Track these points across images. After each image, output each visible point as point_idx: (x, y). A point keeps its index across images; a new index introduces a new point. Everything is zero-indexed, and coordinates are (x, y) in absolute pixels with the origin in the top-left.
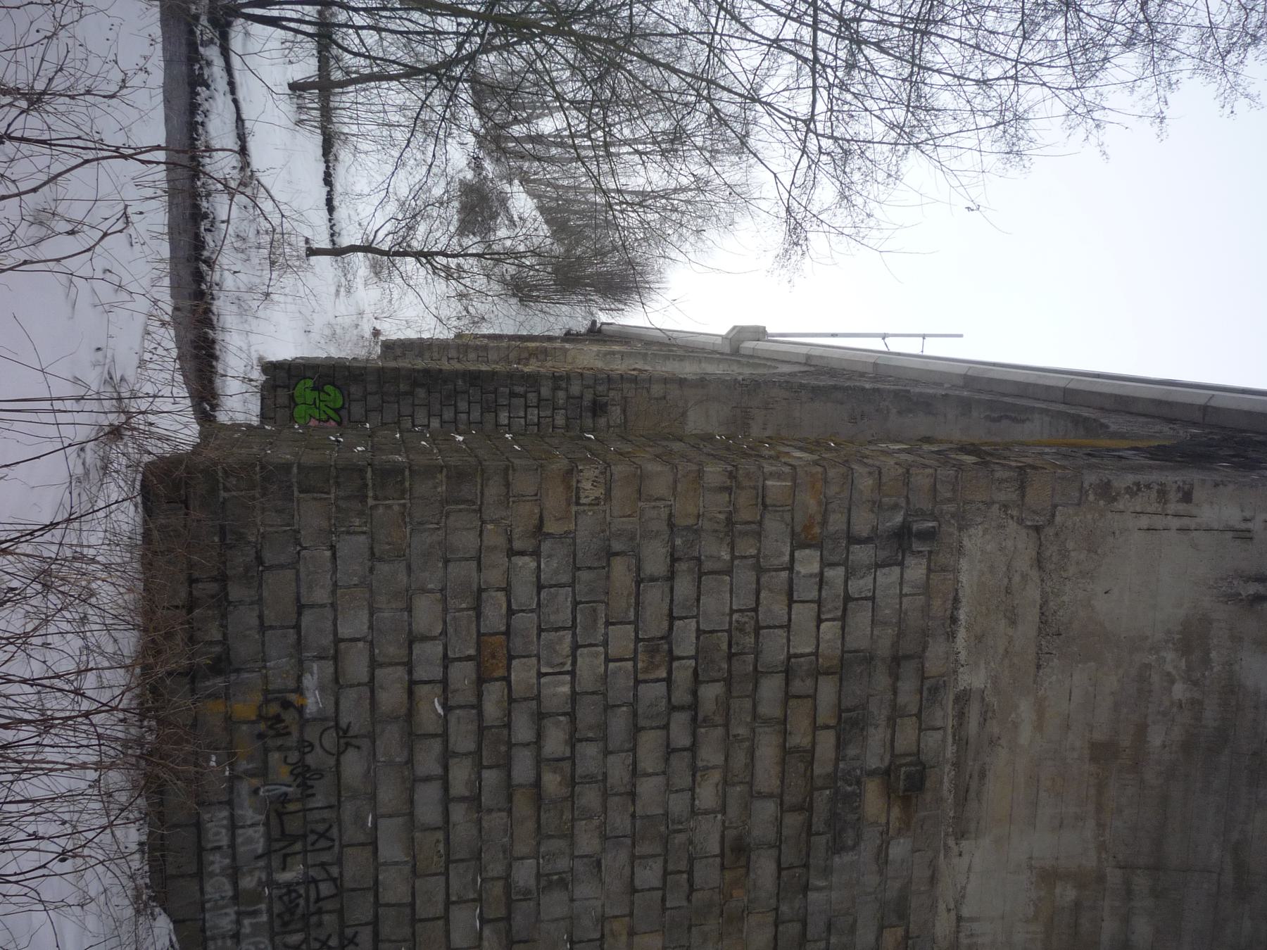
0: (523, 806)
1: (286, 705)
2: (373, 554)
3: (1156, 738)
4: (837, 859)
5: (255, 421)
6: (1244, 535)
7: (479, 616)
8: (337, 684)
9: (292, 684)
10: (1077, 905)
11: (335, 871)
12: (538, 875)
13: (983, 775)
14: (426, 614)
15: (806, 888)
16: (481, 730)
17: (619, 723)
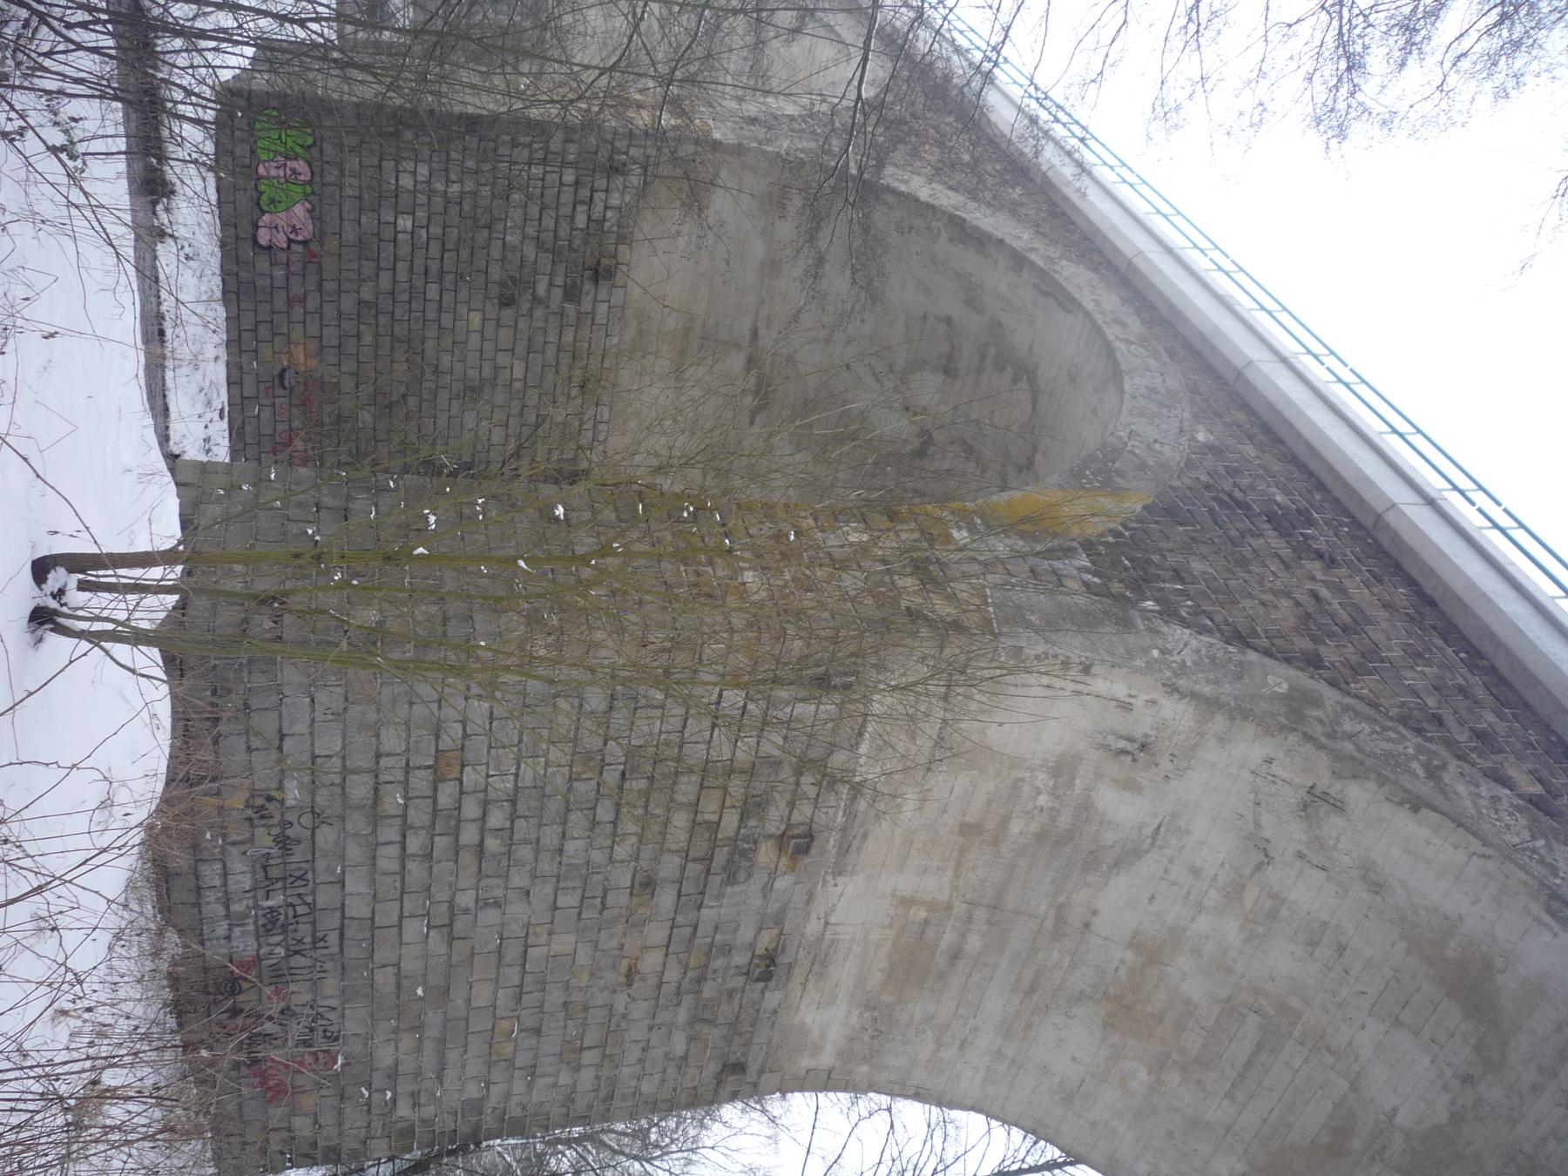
0: (467, 858)
1: (269, 799)
2: (347, 700)
3: (1016, 827)
4: (729, 889)
6: (1126, 707)
7: (437, 738)
8: (313, 787)
9: (274, 785)
10: (926, 922)
11: (309, 899)
12: (477, 900)
13: (865, 836)
14: (392, 740)
15: (700, 906)
16: (435, 812)
17: (554, 806)
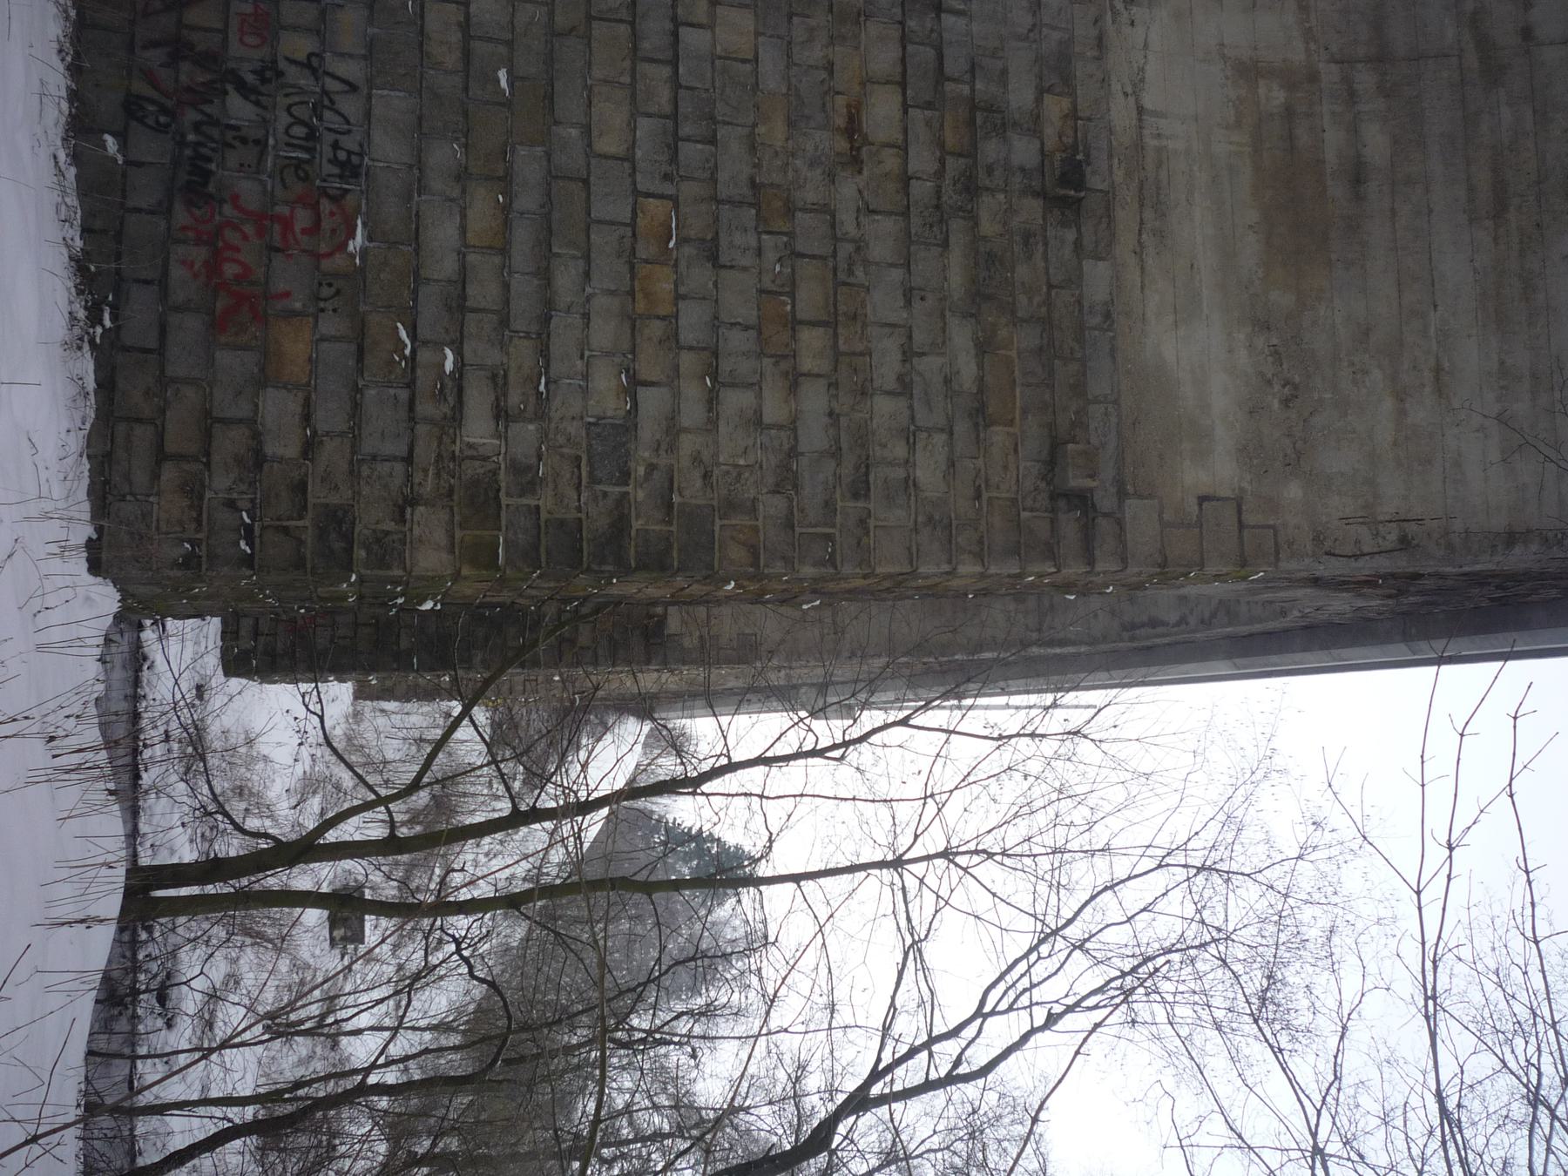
5: (215, 624)
10: (1289, 112)
